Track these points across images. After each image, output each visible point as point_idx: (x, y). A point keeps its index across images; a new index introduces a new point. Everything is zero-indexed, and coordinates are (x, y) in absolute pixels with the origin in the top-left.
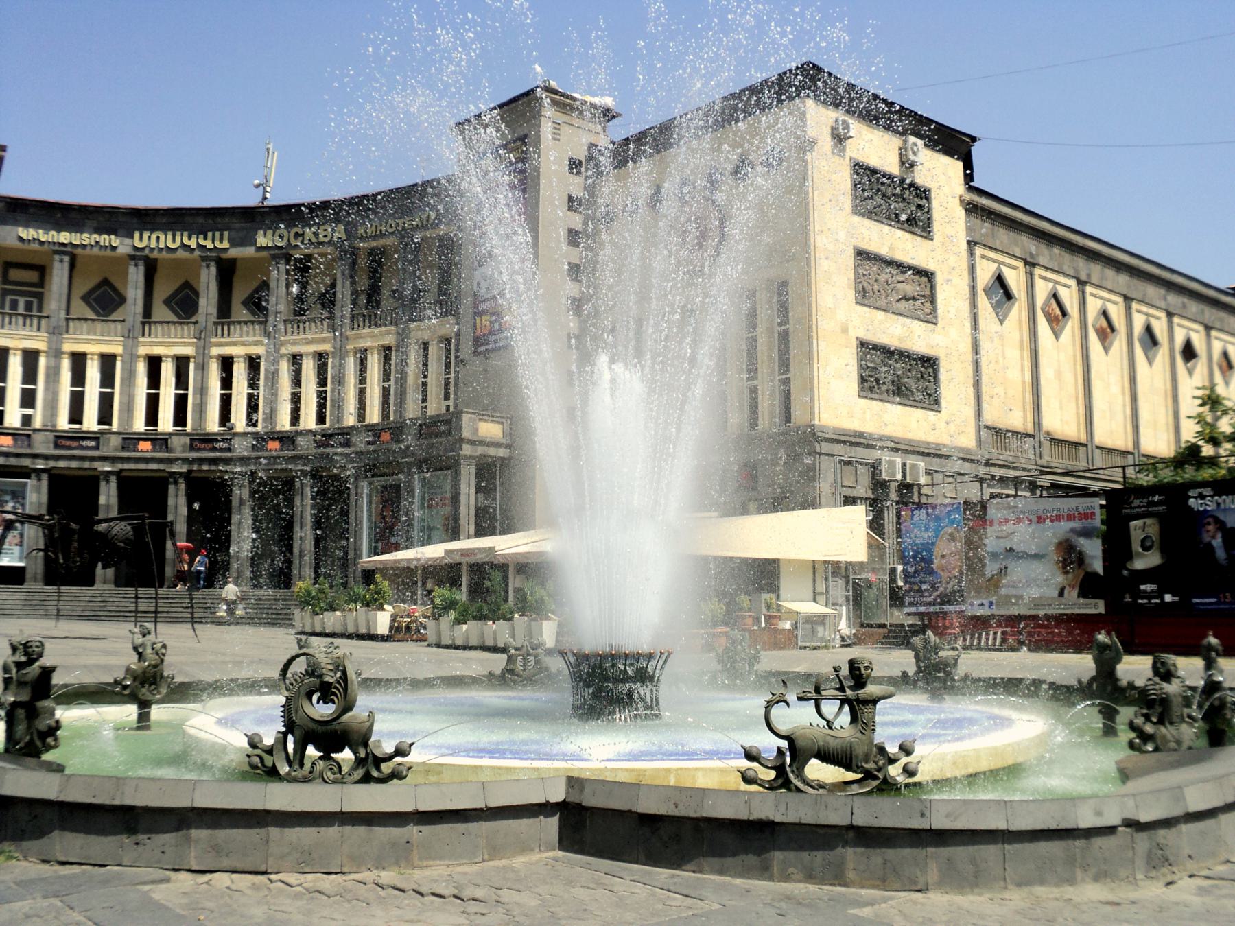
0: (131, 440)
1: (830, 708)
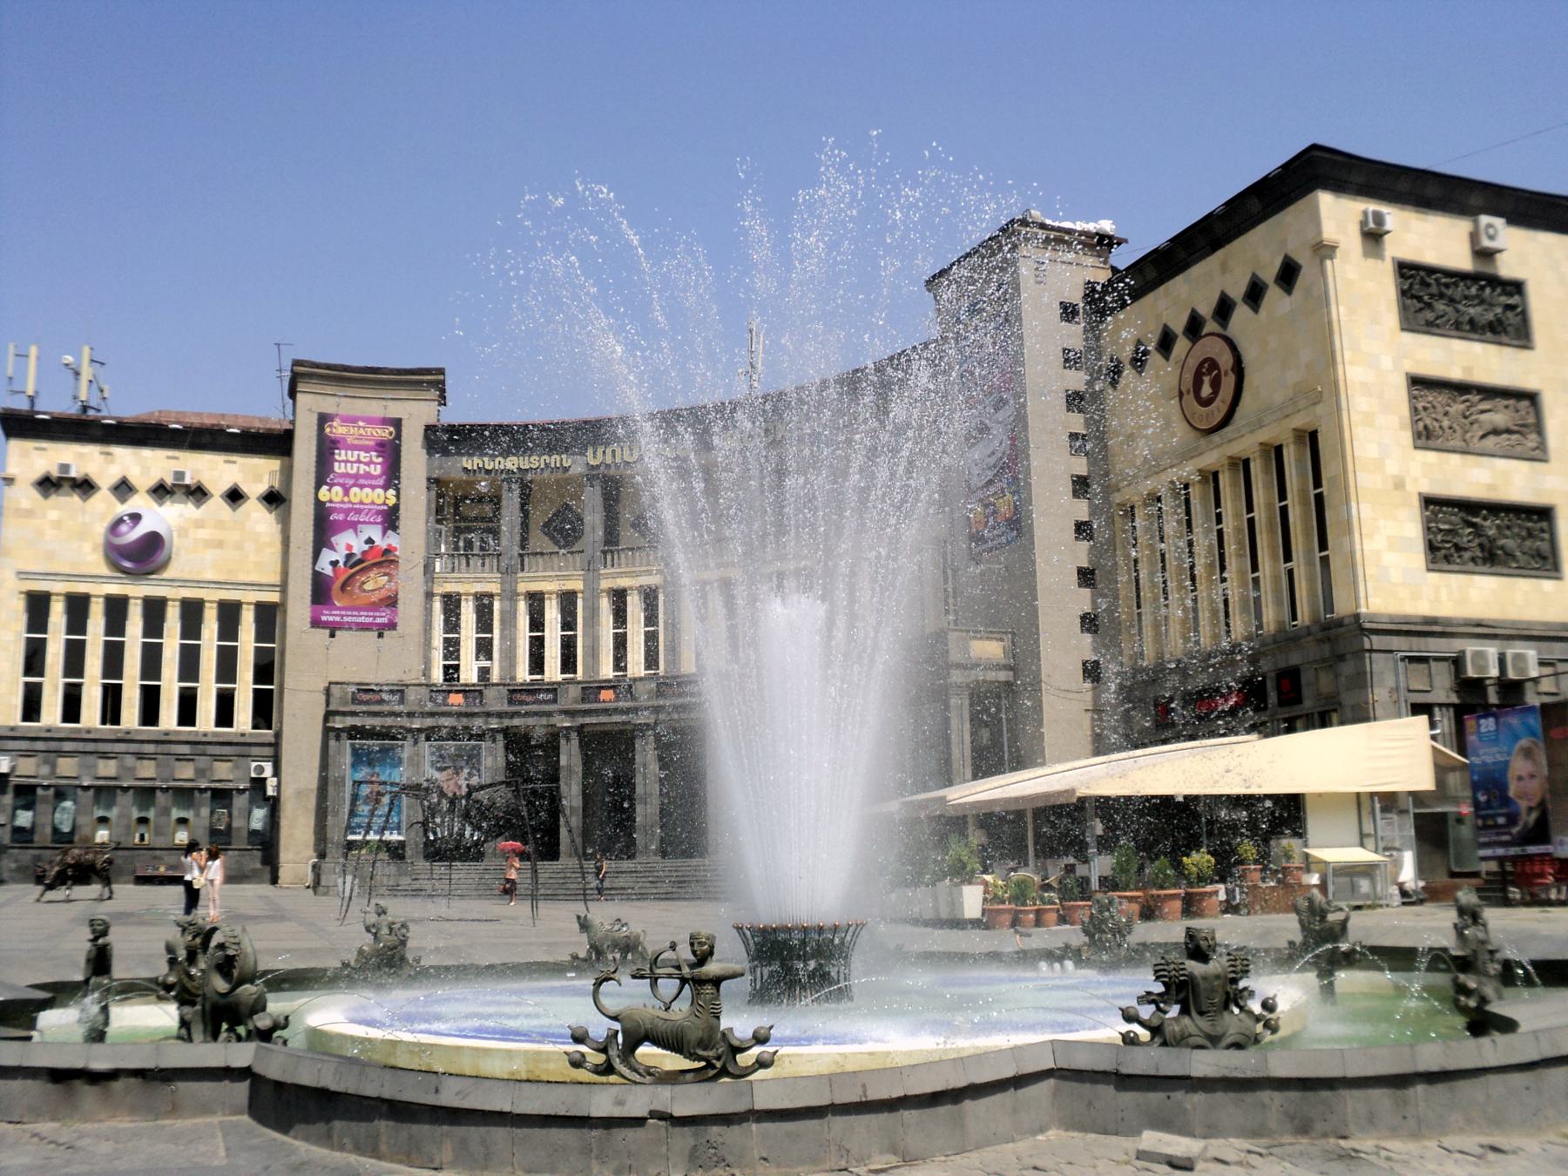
0: (591, 690)
1: (668, 987)
